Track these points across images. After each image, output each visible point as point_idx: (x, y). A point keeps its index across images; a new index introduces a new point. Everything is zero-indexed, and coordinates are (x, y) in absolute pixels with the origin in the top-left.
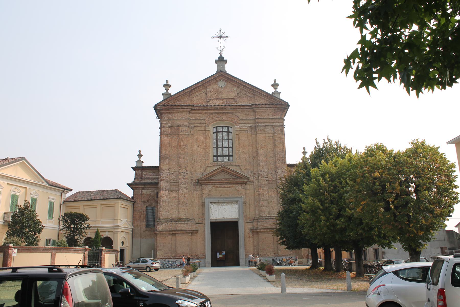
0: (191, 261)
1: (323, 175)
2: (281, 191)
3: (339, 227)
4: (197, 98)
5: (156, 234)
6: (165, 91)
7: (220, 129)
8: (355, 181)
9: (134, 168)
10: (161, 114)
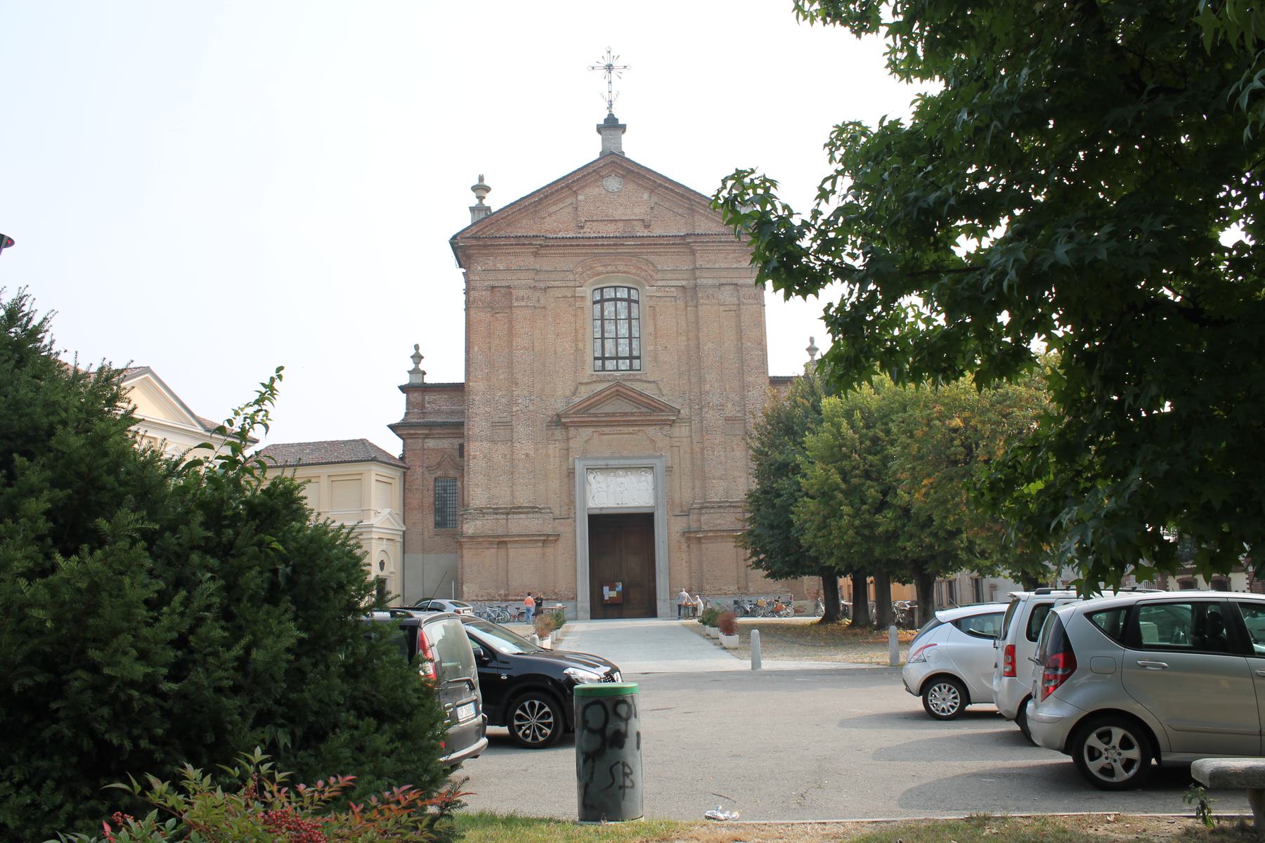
0: (544, 605)
1: (849, 414)
2: (757, 444)
3: (881, 529)
4: (554, 218)
5: (460, 544)
6: (477, 201)
7: (609, 294)
8: (912, 436)
10: (469, 257)
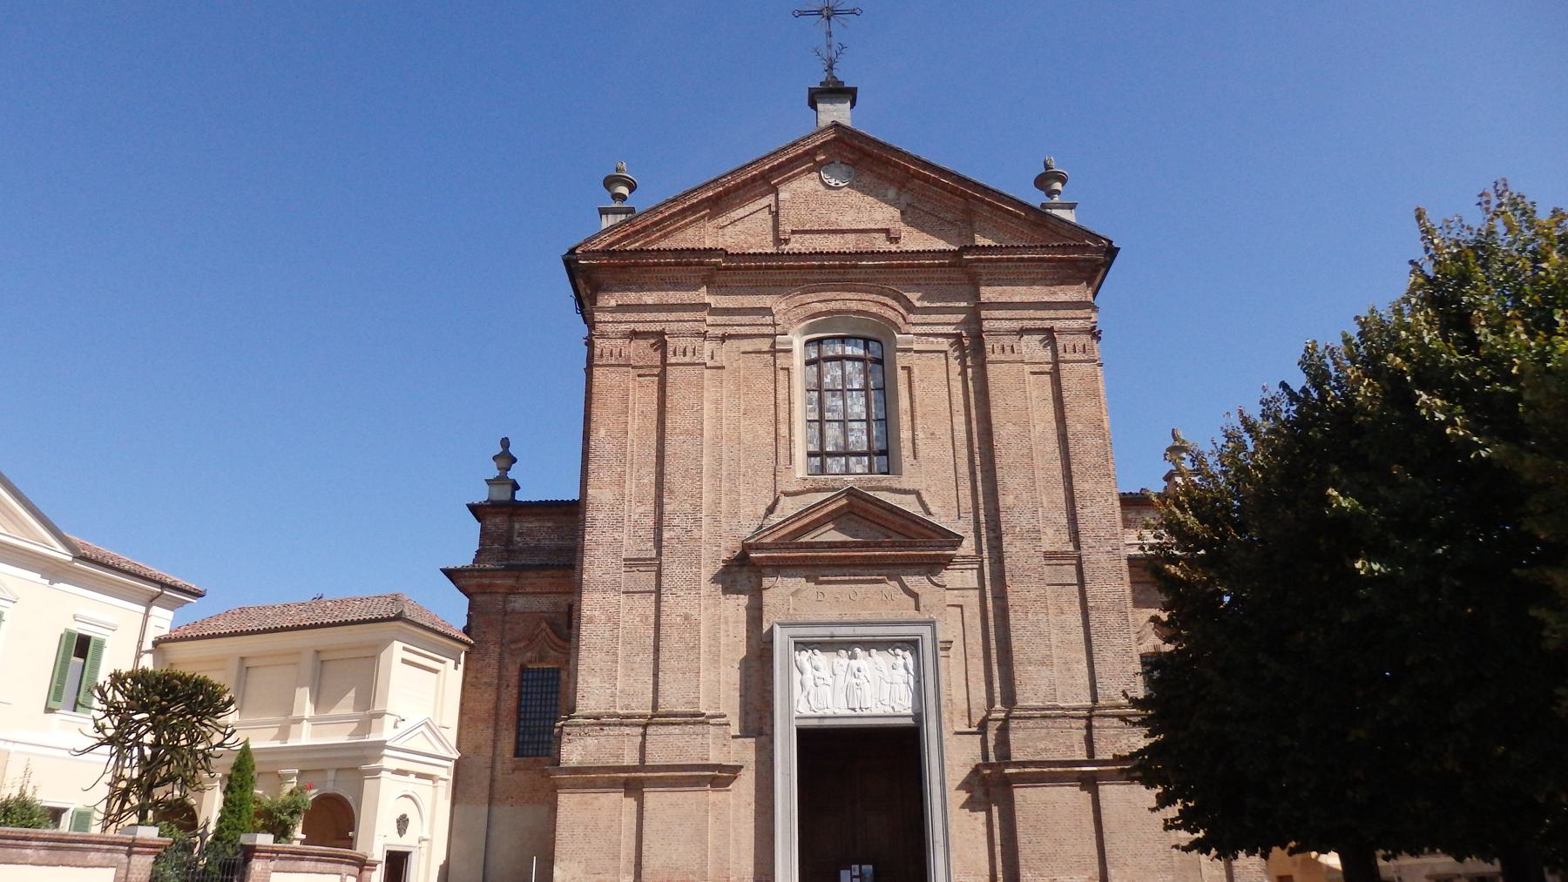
4: (740, 226)
9: (474, 509)
